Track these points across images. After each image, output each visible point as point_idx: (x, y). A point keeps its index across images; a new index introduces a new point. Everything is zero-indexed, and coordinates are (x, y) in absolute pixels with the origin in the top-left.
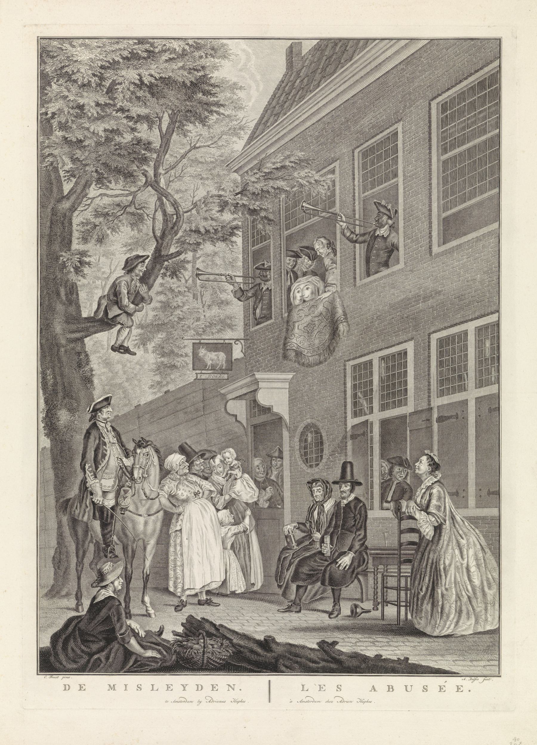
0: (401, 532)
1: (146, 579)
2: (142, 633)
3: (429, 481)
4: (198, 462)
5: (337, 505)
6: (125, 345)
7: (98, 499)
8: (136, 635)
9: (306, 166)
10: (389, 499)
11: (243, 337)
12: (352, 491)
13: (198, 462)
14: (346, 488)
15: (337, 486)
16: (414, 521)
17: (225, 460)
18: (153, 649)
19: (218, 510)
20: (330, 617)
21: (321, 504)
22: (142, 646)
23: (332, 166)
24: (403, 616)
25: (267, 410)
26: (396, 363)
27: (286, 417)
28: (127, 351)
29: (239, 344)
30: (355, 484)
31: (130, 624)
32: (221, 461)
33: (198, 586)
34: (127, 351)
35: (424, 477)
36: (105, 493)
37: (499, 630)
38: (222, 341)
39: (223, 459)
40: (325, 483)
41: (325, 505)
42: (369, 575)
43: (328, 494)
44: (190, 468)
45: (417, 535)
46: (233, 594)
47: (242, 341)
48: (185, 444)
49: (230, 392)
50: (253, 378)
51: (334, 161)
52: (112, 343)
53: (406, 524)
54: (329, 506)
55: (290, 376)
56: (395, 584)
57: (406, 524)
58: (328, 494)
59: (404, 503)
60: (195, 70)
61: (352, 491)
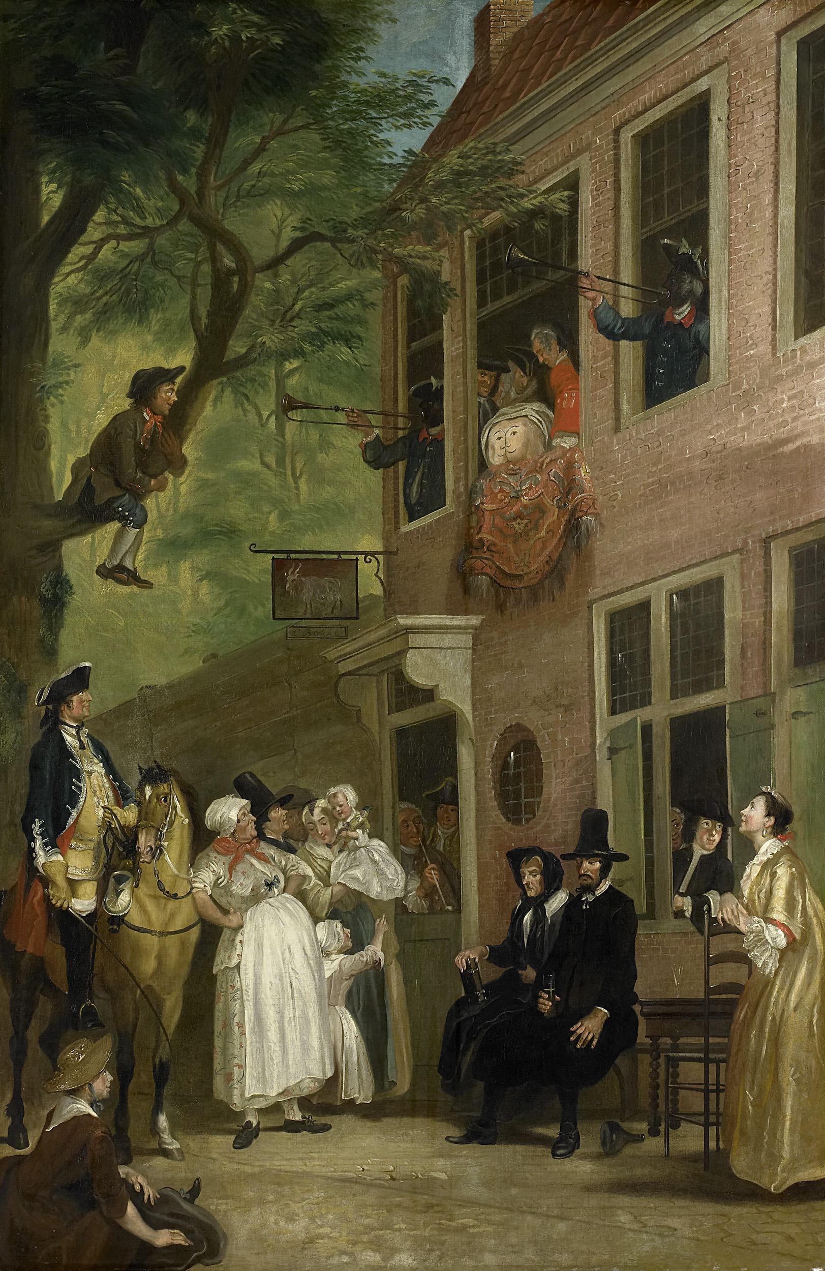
0: (709, 962)
3: (768, 847)
4: (277, 814)
5: (573, 904)
6: (128, 564)
7: (59, 896)
8: (137, 1197)
12: (604, 872)
13: (277, 814)
14: (591, 867)
17: (335, 808)
18: (172, 1226)
19: (316, 920)
21: (539, 903)
22: (147, 1219)
23: (571, 167)
24: (712, 1145)
25: (429, 695)
26: (691, 634)
27: (465, 708)
28: (133, 578)
30: (609, 860)
34: (133, 578)
35: (759, 838)
36: (73, 885)
38: (336, 556)
39: (330, 807)
41: (546, 906)
43: (551, 883)
44: (259, 826)
45: (745, 969)
46: (350, 1107)
50: (383, 926)
51: (579, 152)
53: (720, 945)
54: (557, 902)
55: (474, 621)
56: (700, 1066)
57: (720, 945)
58: (551, 883)
59: (713, 897)
60: (330, 1197)
61: (604, 872)
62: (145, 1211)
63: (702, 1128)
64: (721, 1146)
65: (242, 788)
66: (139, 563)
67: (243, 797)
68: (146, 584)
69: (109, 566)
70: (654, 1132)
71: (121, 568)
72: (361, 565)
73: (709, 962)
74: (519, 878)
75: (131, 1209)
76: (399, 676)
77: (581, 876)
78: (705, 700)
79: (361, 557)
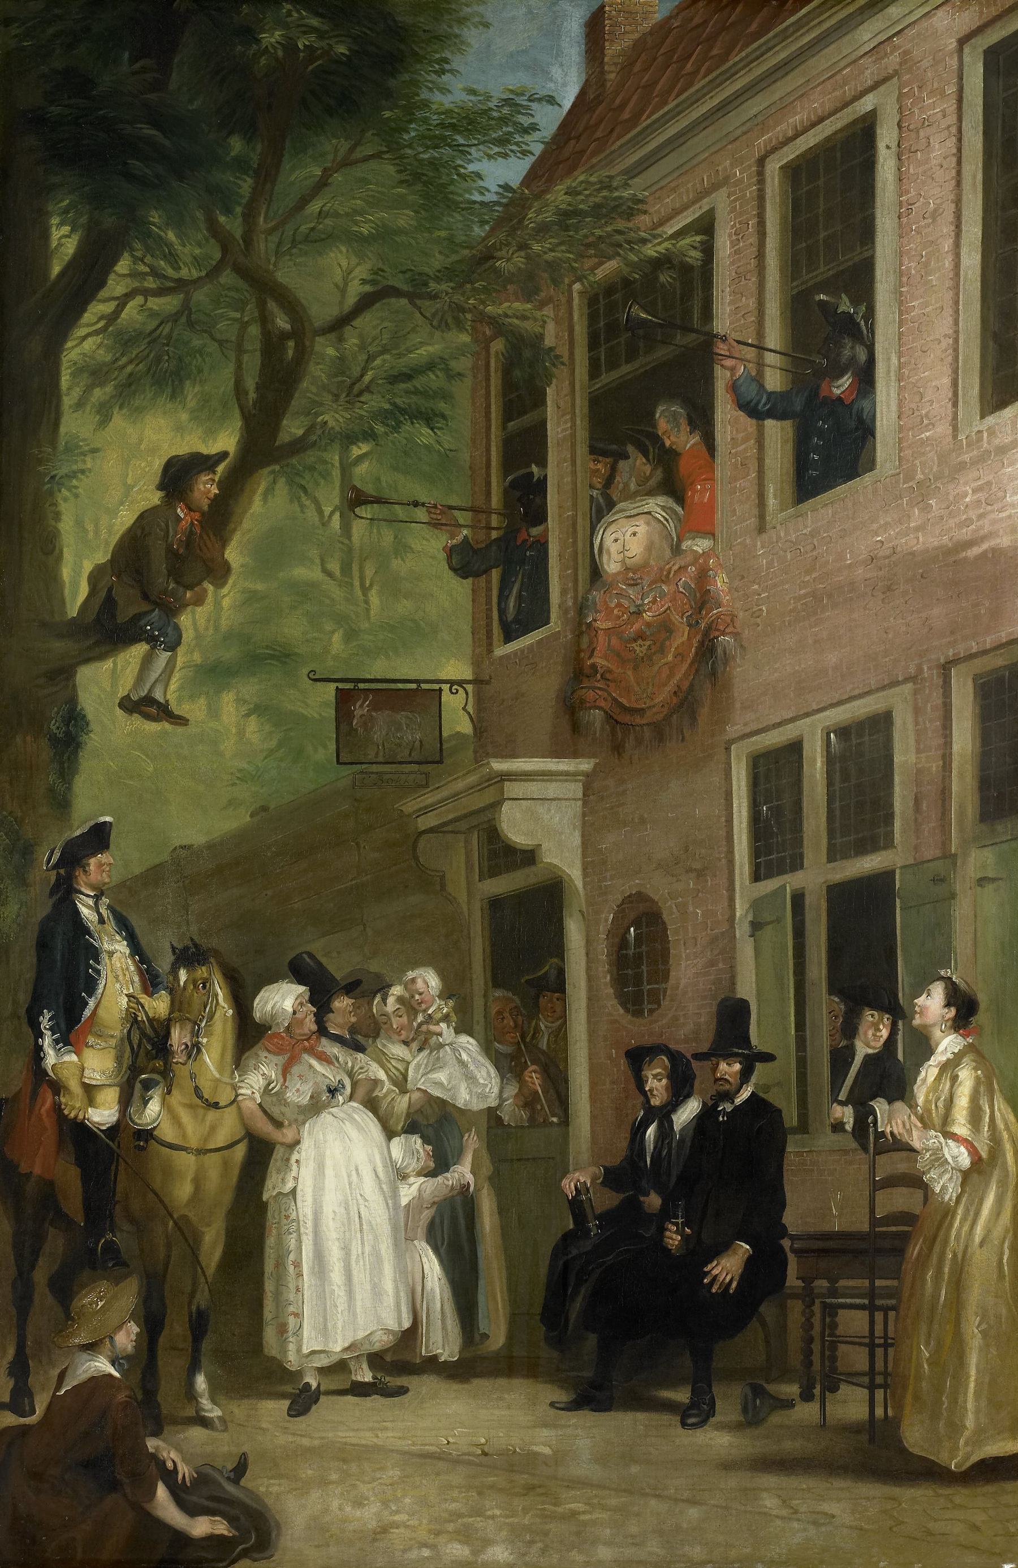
0: (876, 1187)
1: (199, 1325)
2: (184, 1470)
4: (342, 1003)
5: (706, 1116)
6: (158, 695)
7: (73, 1105)
8: (169, 1476)
9: (453, 127)
10: (842, 1096)
11: (470, 677)
12: (745, 1075)
13: (342, 1003)
14: (730, 1069)
15: (708, 1064)
16: (904, 1154)
20: (684, 1424)
21: (664, 1114)
23: (705, 205)
28: (163, 712)
29: (461, 690)
31: (157, 1448)
32: (400, 1000)
33: (337, 1346)
34: (163, 712)
35: (937, 1033)
36: (90, 1091)
37: (874, 1187)
38: (414, 686)
39: (407, 995)
40: (675, 1057)
41: (674, 1117)
42: (790, 1303)
44: (320, 1019)
45: (919, 1194)
46: (432, 1365)
47: (470, 688)
48: (305, 956)
49: (425, 810)
52: (121, 693)
55: (585, 765)
57: (888, 1165)
61: (745, 1075)
62: (179, 1494)
63: (866, 1391)
64: (890, 1413)
65: (299, 972)
66: (171, 693)
67: (300, 982)
68: (180, 721)
69: (135, 697)
70: (807, 1396)
71: (149, 700)
72: (446, 696)
73: (876, 1187)
74: (640, 1082)
75: (162, 1492)
76: (493, 834)
77: (717, 1080)
78: (869, 864)
79: (446, 687)
